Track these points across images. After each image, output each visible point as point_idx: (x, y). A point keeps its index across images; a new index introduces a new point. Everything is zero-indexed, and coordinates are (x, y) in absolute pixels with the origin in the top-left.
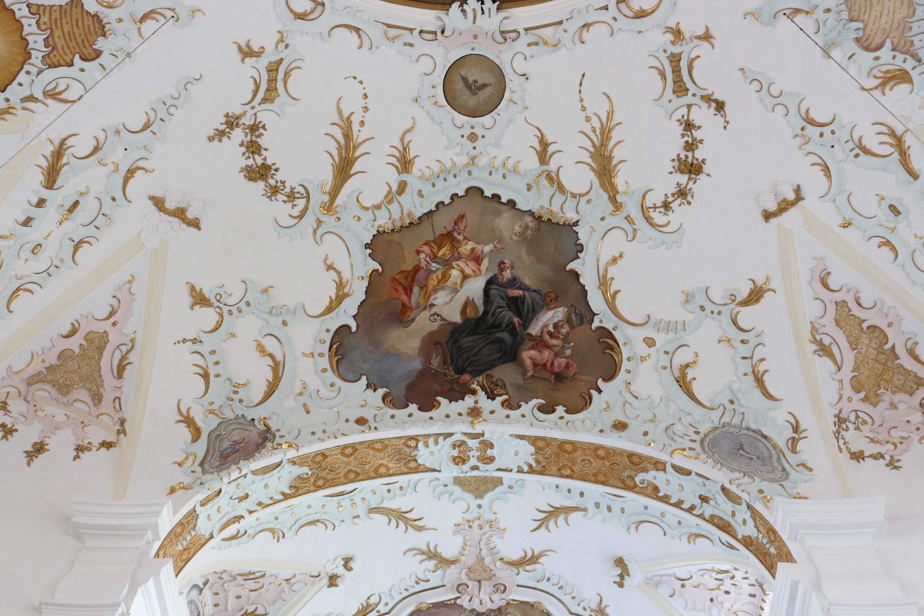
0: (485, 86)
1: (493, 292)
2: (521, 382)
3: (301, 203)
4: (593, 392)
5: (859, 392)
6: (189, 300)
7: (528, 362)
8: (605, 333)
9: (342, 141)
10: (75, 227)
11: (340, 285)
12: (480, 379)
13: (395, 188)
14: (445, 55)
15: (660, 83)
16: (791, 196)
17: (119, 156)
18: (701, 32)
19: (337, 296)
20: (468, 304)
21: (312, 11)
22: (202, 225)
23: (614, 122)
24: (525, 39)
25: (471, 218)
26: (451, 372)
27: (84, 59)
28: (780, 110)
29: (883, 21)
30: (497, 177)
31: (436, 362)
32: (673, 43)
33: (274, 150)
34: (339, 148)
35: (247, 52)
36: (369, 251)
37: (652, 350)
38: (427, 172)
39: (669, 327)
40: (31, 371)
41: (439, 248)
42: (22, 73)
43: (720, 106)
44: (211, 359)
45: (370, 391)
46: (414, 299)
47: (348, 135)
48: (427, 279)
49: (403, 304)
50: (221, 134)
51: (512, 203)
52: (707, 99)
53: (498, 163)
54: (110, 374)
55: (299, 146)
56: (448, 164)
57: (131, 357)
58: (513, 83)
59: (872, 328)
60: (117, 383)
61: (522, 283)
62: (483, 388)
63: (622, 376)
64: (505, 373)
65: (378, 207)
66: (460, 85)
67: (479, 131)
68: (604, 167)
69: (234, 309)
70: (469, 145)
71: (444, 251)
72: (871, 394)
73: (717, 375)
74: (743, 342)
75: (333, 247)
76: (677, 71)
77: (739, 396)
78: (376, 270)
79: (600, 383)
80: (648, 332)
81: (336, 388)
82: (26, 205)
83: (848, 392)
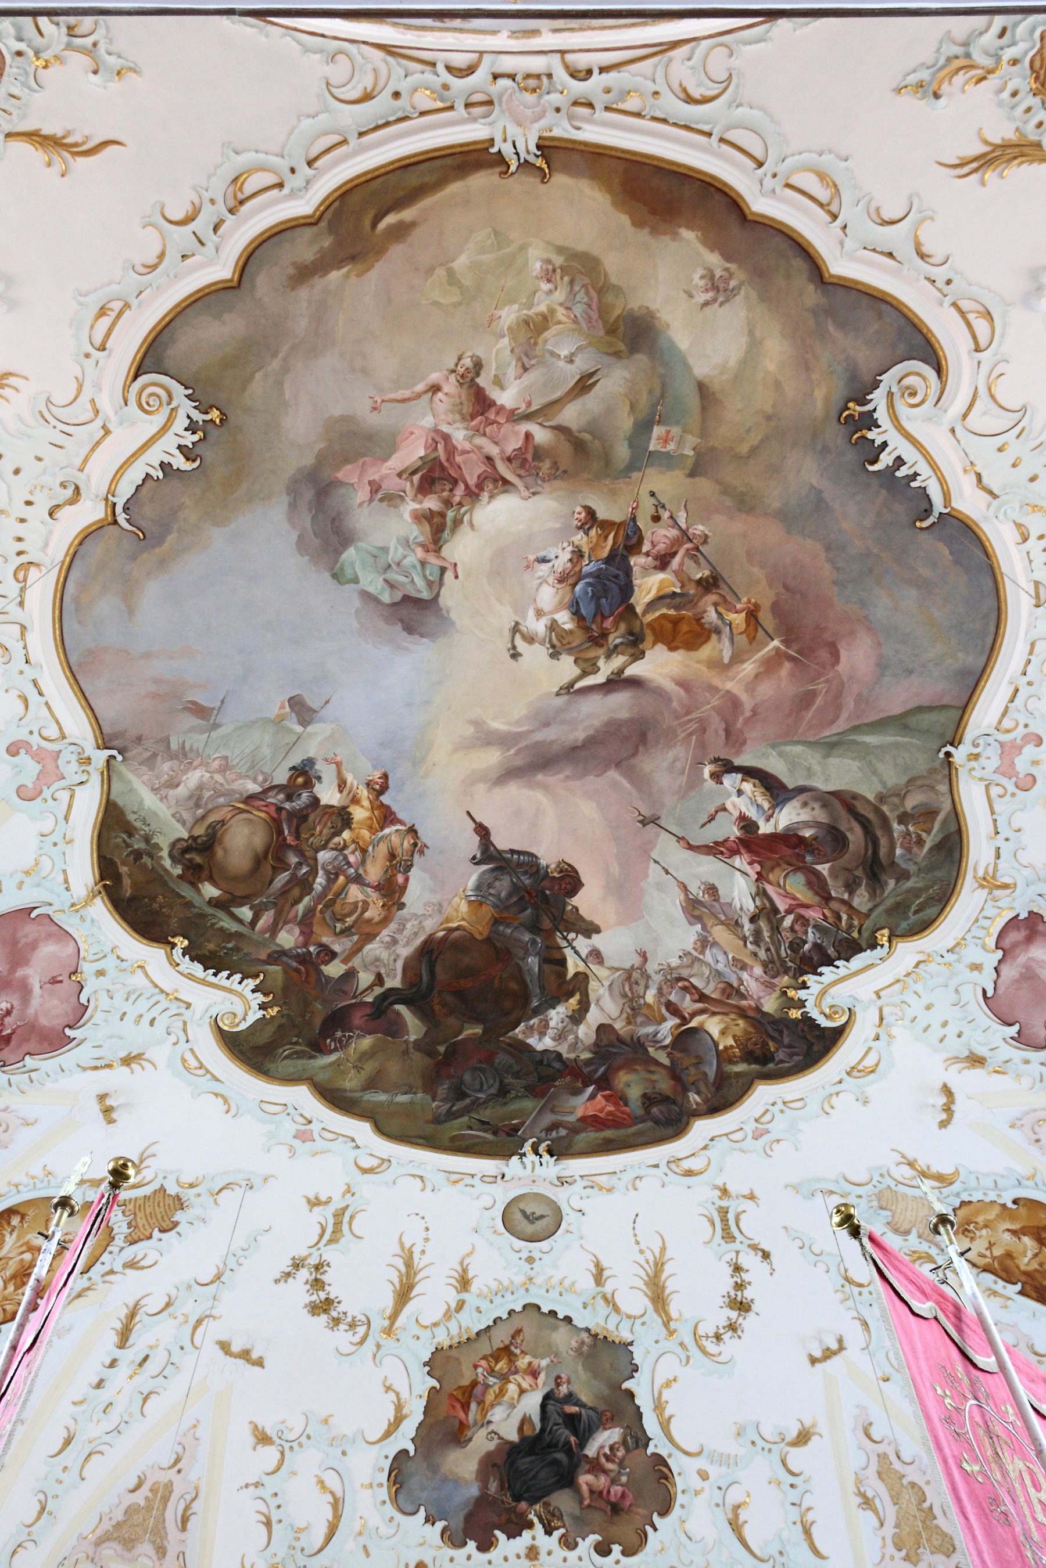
0: (542, 1217)
1: (550, 1408)
2: (577, 1512)
3: (361, 1330)
4: (648, 1528)
5: (900, 1550)
6: (251, 1440)
7: (585, 1488)
8: (660, 1461)
9: (403, 1269)
10: (144, 1381)
11: (399, 1407)
12: (537, 1507)
13: (453, 1305)
14: (502, 1195)
15: (711, 1229)
16: (834, 1346)
17: (189, 1308)
18: (747, 1192)
19: (396, 1418)
20: (525, 1421)
21: (379, 1166)
22: (266, 1364)
23: (666, 1258)
24: (581, 1183)
25: (528, 1332)
26: (508, 1499)
27: (162, 1231)
28: (821, 1267)
29: (908, 1214)
30: (554, 1294)
31: (493, 1487)
32: (720, 1198)
33: (336, 1285)
34: (400, 1277)
35: (315, 1203)
36: (427, 1368)
37: (705, 1484)
38: (485, 1290)
39: (724, 1460)
40: (99, 1532)
41: (497, 1362)
42: (106, 1254)
43: (766, 1255)
44: (273, 1502)
45: (428, 1526)
46: (471, 1416)
47: (409, 1264)
48: (484, 1394)
49: (461, 1423)
51: (568, 1320)
52: (754, 1247)
53: (555, 1281)
54: (174, 1525)
55: (361, 1281)
56: (506, 1283)
57: (196, 1507)
58: (570, 1218)
59: (913, 1485)
60: (182, 1536)
61: (579, 1400)
62: (541, 1521)
63: (676, 1512)
64: (562, 1500)
65: (435, 1325)
66: (518, 1216)
67: (536, 1255)
68: (659, 1298)
69: (295, 1445)
70: (528, 1266)
71: (502, 1366)
72: (912, 1553)
74: (792, 1486)
75: (392, 1370)
76: (724, 1220)
77: (788, 1548)
78: (434, 1388)
79: (655, 1517)
80: (701, 1463)
81: (395, 1523)
82: (100, 1367)
83: (891, 1549)
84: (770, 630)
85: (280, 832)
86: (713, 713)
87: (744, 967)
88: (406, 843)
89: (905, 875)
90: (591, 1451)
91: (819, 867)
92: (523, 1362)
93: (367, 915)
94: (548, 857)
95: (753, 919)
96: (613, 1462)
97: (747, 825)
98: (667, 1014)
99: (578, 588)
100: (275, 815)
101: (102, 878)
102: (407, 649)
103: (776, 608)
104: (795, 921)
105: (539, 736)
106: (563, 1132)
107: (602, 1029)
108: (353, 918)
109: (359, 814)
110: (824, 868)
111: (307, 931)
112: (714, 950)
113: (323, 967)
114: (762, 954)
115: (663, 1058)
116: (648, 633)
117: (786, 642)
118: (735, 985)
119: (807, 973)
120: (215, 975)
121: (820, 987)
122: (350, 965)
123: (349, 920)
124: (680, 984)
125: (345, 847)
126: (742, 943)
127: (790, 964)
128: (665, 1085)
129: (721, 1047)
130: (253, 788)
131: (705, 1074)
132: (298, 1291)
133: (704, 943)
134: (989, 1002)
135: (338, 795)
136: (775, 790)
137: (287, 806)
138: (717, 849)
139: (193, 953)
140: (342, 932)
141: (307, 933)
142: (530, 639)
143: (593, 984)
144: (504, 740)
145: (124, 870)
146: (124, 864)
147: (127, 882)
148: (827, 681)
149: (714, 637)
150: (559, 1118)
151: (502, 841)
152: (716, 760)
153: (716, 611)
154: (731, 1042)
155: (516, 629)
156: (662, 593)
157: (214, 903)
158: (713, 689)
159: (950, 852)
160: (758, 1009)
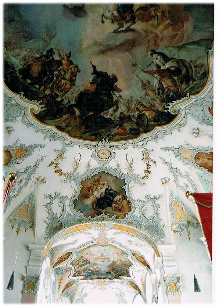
7: (113, 207)
15: (143, 157)
25: (103, 177)
41: (96, 183)
43: (155, 162)
46: (90, 193)
49: (88, 194)
50: (50, 165)
62: (104, 213)
64: (109, 209)
73: (150, 213)
84: (167, 17)
85: (45, 67)
86: (151, 39)
87: (155, 100)
88: (75, 70)
89: (194, 80)
90: (115, 200)
91: (174, 78)
92: (101, 183)
93: (66, 87)
94: (110, 74)
95: (158, 89)
96: (120, 202)
97: (158, 67)
98: (136, 111)
99: (119, 5)
100: (43, 62)
101: (3, 78)
102: (76, 20)
103: (169, 12)
104: (168, 90)
105: (108, 43)
106: (111, 136)
107: (121, 113)
108: (63, 87)
109: (64, 62)
110: (176, 78)
111: (52, 90)
112: (148, 96)
113: (56, 99)
114: (160, 98)
115: (135, 120)
116: (136, 17)
117: (171, 21)
118: (153, 104)
119: (170, 102)
120: (31, 101)
121: (172, 105)
122: (62, 98)
123: (62, 88)
124: (140, 104)
125: (61, 70)
126: (155, 95)
127: (166, 100)
128: (135, 127)
129: (148, 118)
130: (38, 56)
131: (144, 124)
132: (53, 168)
133: (146, 94)
134: (210, 110)
135: (59, 58)
136: (166, 59)
137: (46, 60)
138: (151, 73)
139: (26, 96)
140: (60, 91)
141: (52, 91)
142: (107, 18)
143: (119, 103)
144: (100, 45)
145: (8, 76)
146: (8, 75)
147: (9, 79)
148: (181, 31)
149: (153, 19)
150: (110, 133)
151: (99, 69)
152: (152, 50)
153: (154, 12)
154: (151, 117)
155: (103, 15)
156: (141, 6)
157: (29, 84)
158: (152, 32)
159: (206, 76)
160: (158, 110)
